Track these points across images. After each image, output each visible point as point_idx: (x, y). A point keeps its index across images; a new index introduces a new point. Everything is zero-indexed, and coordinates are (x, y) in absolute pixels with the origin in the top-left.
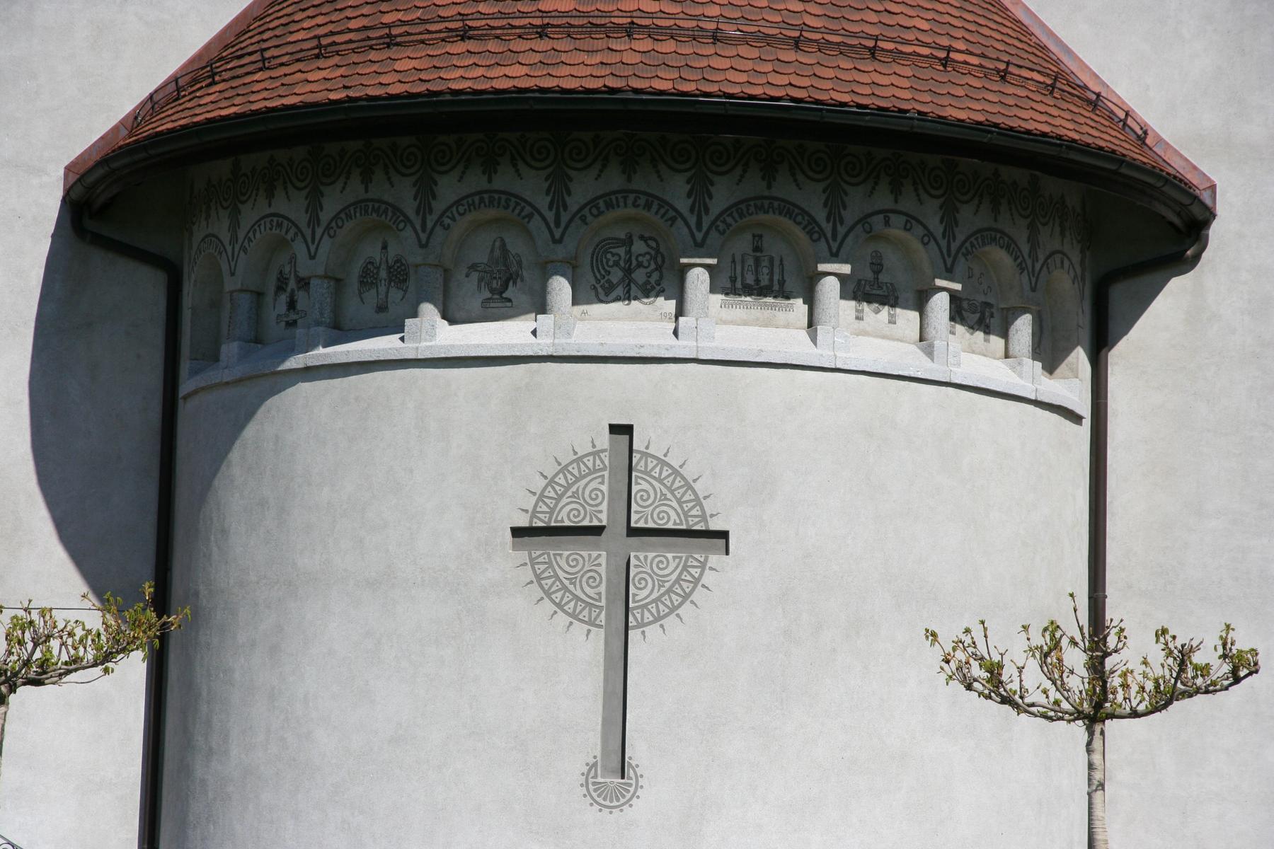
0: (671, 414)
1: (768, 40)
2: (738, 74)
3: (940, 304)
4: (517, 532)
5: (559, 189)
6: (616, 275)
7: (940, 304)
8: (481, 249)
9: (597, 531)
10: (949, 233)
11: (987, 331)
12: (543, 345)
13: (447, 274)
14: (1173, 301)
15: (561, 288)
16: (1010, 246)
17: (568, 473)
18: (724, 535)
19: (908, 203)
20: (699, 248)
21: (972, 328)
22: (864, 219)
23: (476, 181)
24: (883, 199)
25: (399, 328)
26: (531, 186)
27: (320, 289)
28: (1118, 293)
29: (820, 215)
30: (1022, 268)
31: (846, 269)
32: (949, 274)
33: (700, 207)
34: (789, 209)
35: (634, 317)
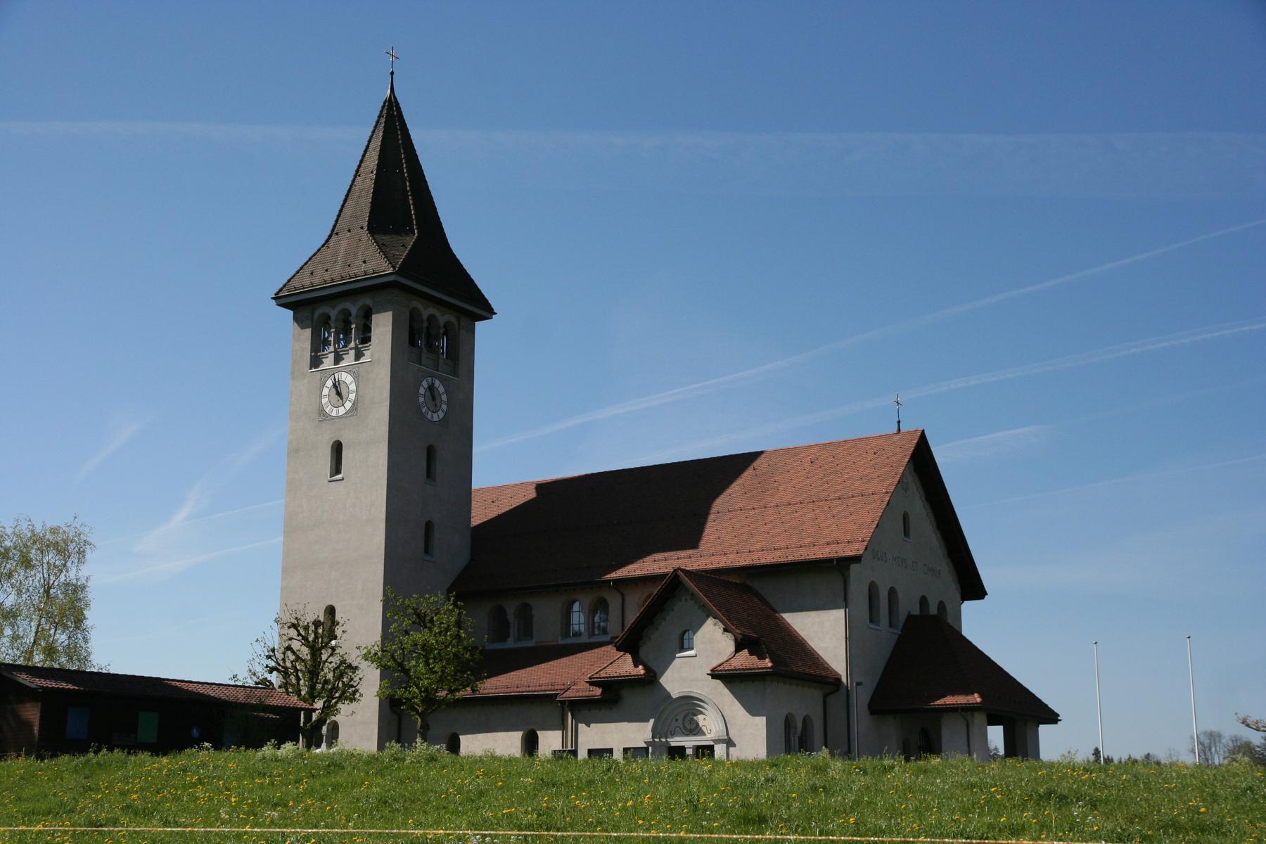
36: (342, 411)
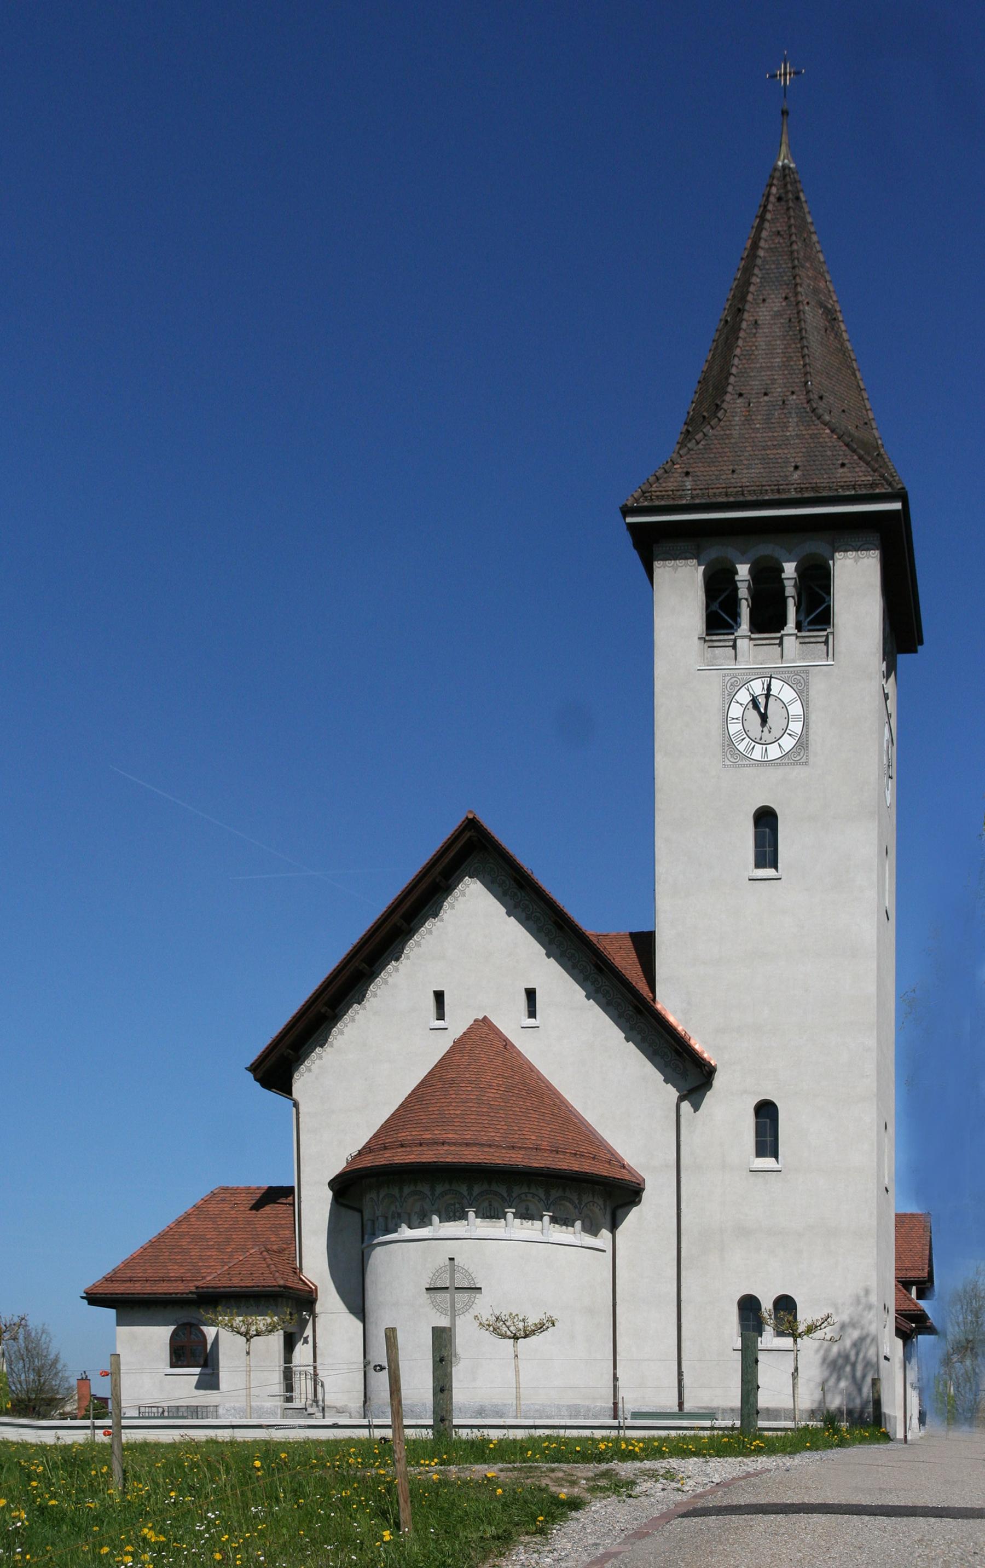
0: (465, 1254)
1: (483, 1145)
2: (517, 1159)
3: (546, 1219)
4: (427, 1289)
5: (433, 1189)
6: (451, 1214)
7: (546, 1219)
8: (417, 1208)
9: (447, 1288)
10: (548, 1199)
11: (567, 1226)
12: (430, 1235)
13: (409, 1215)
14: (634, 1213)
15: (435, 1219)
16: (571, 1201)
17: (438, 1273)
18: (480, 1288)
19: (533, 1190)
20: (471, 1206)
21: (561, 1225)
22: (519, 1196)
23: (412, 1188)
24: (525, 1189)
25: (396, 1231)
26: (426, 1189)
27: (381, 1220)
28: (619, 1212)
29: (505, 1195)
30: (575, 1207)
31: (514, 1210)
32: (548, 1210)
33: (470, 1194)
34: (496, 1194)
35: (456, 1226)
36: (774, 752)
